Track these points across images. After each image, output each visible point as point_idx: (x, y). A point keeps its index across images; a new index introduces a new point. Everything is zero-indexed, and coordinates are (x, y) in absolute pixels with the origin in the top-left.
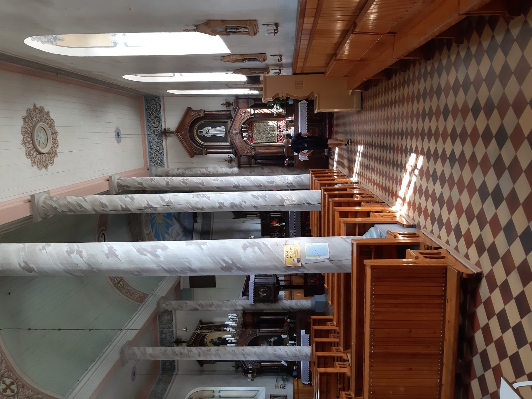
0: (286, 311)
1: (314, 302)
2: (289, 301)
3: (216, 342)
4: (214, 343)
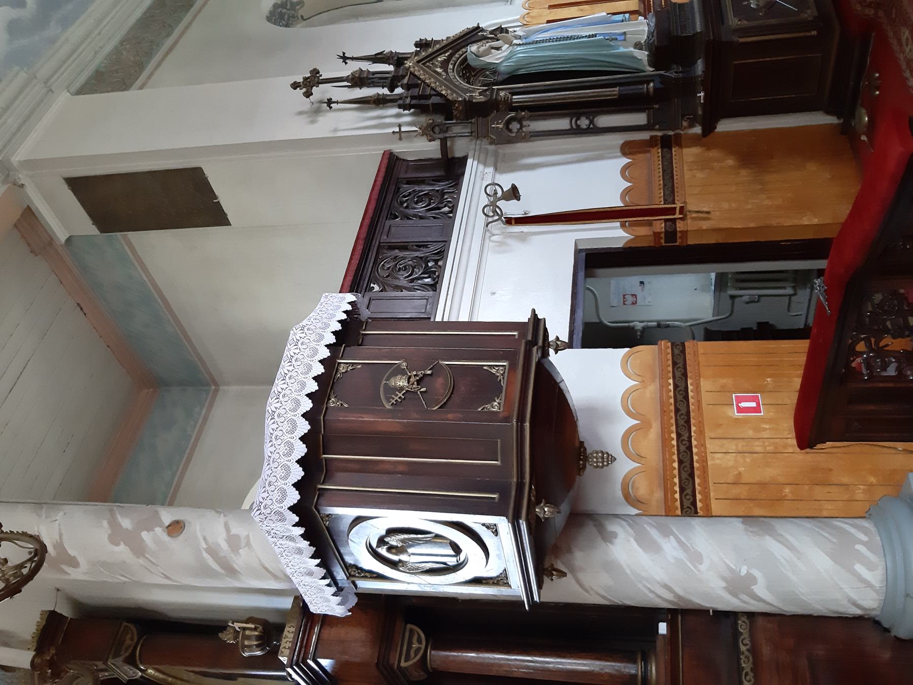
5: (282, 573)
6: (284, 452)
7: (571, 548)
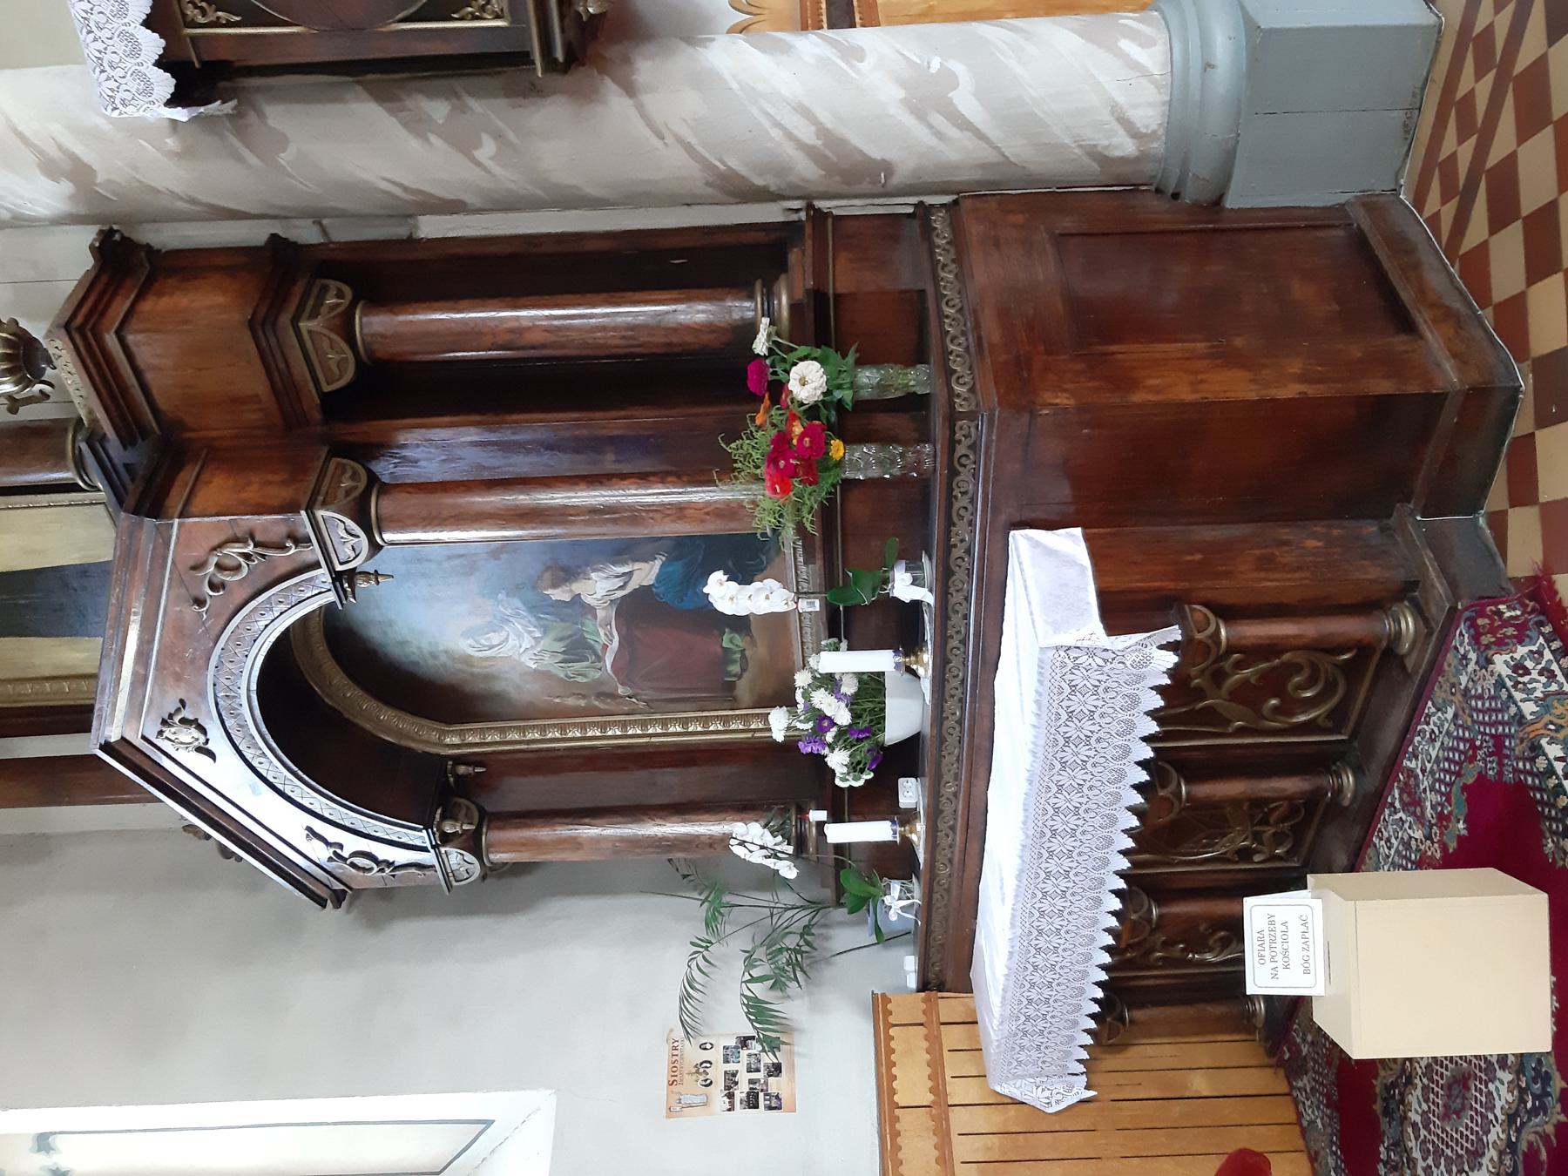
1: (1224, 46)
2: (813, 46)
6: (138, 89)
7: (629, 58)
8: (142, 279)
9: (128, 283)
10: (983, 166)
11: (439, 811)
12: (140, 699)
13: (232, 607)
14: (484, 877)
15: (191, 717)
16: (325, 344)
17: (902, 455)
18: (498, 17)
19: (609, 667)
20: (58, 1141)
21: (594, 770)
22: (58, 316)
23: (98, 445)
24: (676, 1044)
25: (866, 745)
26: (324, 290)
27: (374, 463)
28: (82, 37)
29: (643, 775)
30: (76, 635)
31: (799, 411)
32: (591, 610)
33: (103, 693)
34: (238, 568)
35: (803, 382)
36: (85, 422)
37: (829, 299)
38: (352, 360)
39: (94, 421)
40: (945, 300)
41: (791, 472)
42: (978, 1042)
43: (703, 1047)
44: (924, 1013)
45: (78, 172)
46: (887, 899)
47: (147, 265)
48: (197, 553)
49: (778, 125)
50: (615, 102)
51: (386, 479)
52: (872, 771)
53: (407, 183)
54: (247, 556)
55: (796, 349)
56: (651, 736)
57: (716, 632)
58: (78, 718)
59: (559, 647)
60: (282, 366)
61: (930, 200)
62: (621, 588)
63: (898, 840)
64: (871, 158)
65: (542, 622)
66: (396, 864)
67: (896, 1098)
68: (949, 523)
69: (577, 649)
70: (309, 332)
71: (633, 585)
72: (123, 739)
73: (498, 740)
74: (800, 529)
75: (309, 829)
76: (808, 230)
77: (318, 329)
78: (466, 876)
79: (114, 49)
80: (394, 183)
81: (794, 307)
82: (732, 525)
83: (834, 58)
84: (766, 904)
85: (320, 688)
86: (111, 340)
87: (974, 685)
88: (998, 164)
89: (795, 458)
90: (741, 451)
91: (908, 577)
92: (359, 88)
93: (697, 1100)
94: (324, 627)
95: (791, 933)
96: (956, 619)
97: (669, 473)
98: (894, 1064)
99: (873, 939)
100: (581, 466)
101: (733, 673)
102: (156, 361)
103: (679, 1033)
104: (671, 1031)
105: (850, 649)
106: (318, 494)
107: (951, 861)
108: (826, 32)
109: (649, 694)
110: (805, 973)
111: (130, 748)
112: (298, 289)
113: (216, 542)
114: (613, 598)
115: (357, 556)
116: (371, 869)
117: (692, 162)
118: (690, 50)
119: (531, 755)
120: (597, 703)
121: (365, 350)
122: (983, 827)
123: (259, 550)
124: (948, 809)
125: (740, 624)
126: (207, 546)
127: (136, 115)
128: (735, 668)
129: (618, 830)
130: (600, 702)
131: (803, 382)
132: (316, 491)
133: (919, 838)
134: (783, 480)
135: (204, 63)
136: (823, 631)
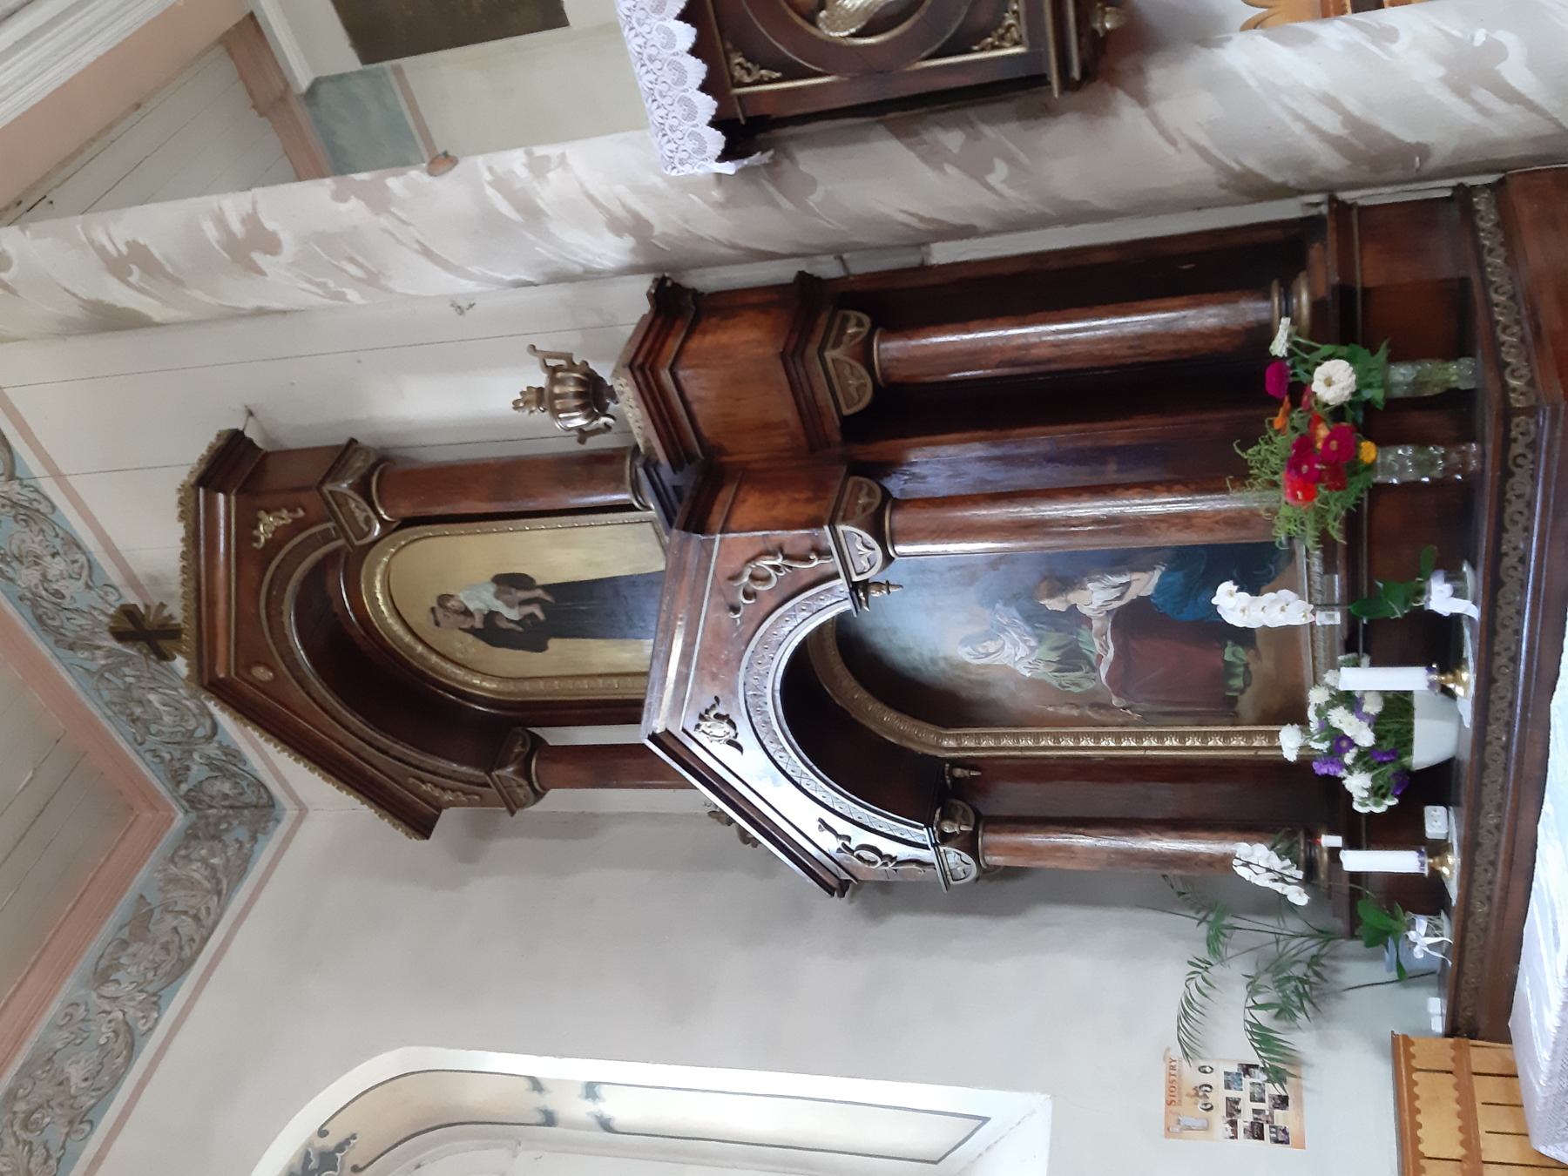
0: (1289, 210)
2: (1338, 33)
3: (491, 616)
4: (478, 624)
5: (618, 202)
8: (691, 317)
9: (679, 323)
10: (1536, 140)
11: (938, 811)
12: (682, 696)
13: (762, 614)
14: (977, 879)
15: (724, 713)
16: (847, 370)
17: (1444, 457)
18: (1016, 44)
19: (1103, 676)
20: (603, 1091)
21: (1089, 780)
22: (621, 357)
23: (652, 470)
24: (1173, 1064)
25: (1390, 769)
26: (846, 320)
27: (887, 479)
28: (647, 106)
29: (1138, 788)
30: (625, 637)
31: (1320, 412)
32: (1087, 620)
33: (652, 688)
34: (767, 579)
35: (1329, 382)
36: (642, 450)
37: (1356, 294)
38: (868, 380)
39: (650, 449)
40: (1495, 286)
41: (1315, 477)
42: (1518, 1097)
43: (1202, 1070)
44: (1453, 1060)
45: (637, 227)
46: (1412, 935)
47: (693, 307)
48: (733, 565)
49: (1299, 118)
50: (1128, 116)
51: (896, 494)
52: (1397, 796)
53: (921, 213)
54: (776, 568)
55: (1318, 349)
56: (1146, 748)
57: (1217, 645)
58: (630, 711)
59: (1054, 656)
60: (808, 391)
61: (1470, 181)
62: (1118, 598)
63: (1426, 872)
64: (1402, 142)
65: (1038, 632)
66: (898, 859)
67: (1421, 1147)
68: (1500, 529)
69: (1072, 658)
70: (833, 360)
71: (1131, 595)
72: (667, 730)
73: (993, 745)
74: (1324, 539)
75: (821, 821)
76: (1330, 224)
77: (842, 358)
78: (963, 876)
79: (674, 115)
80: (911, 214)
81: (1316, 306)
82: (1243, 533)
83: (1364, 42)
84: (1272, 930)
85: (831, 689)
86: (665, 376)
87: (1525, 708)
88: (1553, 136)
89: (1320, 463)
90: (1260, 457)
91: (1447, 588)
92: (880, 128)
93: (1199, 1124)
94: (836, 631)
95: (1300, 961)
96: (1504, 635)
97: (1178, 482)
98: (1419, 1111)
99: (1394, 975)
100: (1083, 476)
101: (1235, 687)
102: (702, 394)
103: (1177, 1052)
104: (1168, 1049)
105: (1373, 664)
106: (838, 510)
107: (1489, 898)
108: (1350, 16)
109: (1147, 707)
110: (1312, 1003)
111: (673, 740)
112: (823, 320)
113: (750, 554)
114: (1110, 608)
115: (871, 568)
116: (875, 863)
117: (1205, 165)
118: (1204, 52)
119: (1024, 762)
120: (1090, 713)
121: (882, 374)
122: (1530, 864)
123: (787, 563)
124: (1487, 841)
125: (1244, 636)
126: (742, 560)
127: (691, 172)
128: (1237, 683)
129: (1113, 842)
130: (1094, 711)
131: (1329, 382)
132: (836, 509)
133: (1451, 872)
134: (1306, 485)
135: (748, 119)
136: (1338, 647)
